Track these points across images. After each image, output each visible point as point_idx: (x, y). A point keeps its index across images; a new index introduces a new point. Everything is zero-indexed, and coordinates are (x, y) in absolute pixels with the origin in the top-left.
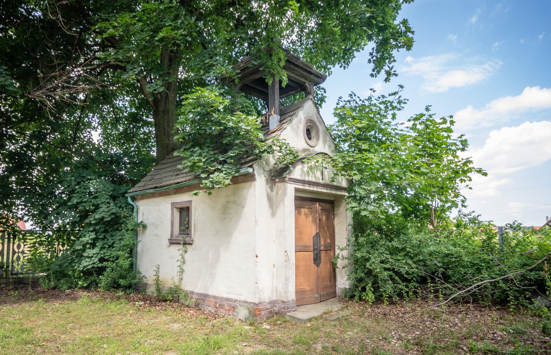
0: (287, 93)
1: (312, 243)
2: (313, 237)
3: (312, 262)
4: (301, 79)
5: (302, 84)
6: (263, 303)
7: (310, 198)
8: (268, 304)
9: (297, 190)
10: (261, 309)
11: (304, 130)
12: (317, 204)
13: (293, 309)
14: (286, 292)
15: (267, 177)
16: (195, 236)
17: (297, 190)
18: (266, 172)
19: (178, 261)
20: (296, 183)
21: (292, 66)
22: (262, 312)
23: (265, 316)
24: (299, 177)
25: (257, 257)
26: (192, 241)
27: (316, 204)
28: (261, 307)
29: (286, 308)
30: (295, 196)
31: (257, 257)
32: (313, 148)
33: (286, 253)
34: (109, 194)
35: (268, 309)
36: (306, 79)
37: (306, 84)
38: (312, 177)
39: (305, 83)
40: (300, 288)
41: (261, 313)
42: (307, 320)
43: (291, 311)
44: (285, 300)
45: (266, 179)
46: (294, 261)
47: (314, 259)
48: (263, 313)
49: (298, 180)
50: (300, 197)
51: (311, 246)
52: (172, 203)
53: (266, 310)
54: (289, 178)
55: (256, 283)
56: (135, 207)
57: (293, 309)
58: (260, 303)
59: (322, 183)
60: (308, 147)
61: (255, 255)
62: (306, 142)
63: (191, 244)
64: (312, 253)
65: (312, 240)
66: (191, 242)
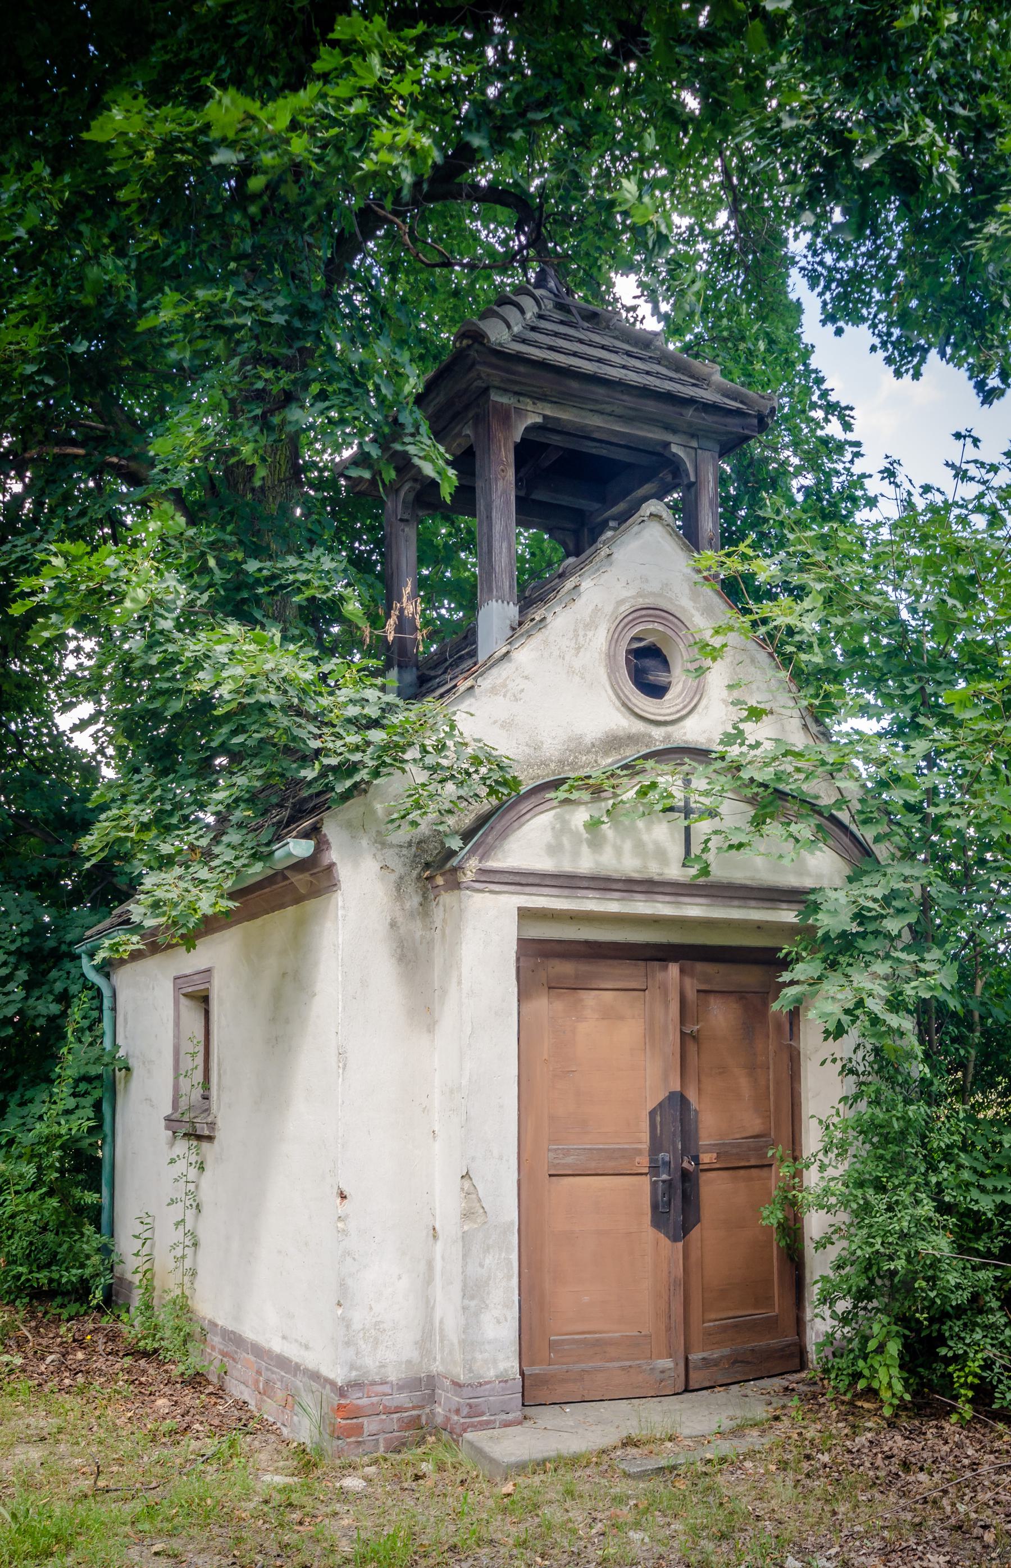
0: (628, 493)
1: (646, 1137)
2: (652, 1114)
3: (647, 1218)
4: (650, 435)
5: (659, 449)
6: (373, 1383)
7: (647, 946)
8: (401, 1388)
9: (525, 915)
10: (359, 1408)
11: (611, 658)
12: (673, 970)
13: (504, 1417)
14: (469, 1343)
15: (400, 870)
16: (219, 1109)
17: (525, 915)
18: (390, 852)
19: (172, 1202)
20: (528, 889)
21: (574, 385)
22: (365, 1421)
23: (381, 1438)
24: (545, 864)
25: (343, 1197)
26: (212, 1125)
27: (666, 968)
28: (365, 1401)
29: (465, 1411)
30: (521, 941)
31: (343, 1197)
32: (669, 729)
33: (467, 1184)
34: (13, 948)
35: (398, 1410)
36: (668, 428)
37: (674, 449)
38: (618, 851)
39: (667, 445)
40: (580, 1328)
41: (360, 1427)
42: (510, 1466)
43: (488, 1422)
44: (462, 1379)
45: (394, 877)
46: (512, 1215)
47: (655, 1207)
48: (370, 1425)
49: (544, 875)
50: (587, 943)
51: (638, 1152)
52: (176, 978)
53: (389, 1412)
54: (482, 871)
55: (339, 1304)
56: (106, 993)
57: (504, 1417)
58: (356, 1385)
59: (682, 879)
60: (639, 727)
61: (335, 1190)
62: (624, 704)
63: (210, 1138)
64: (645, 1182)
65: (645, 1125)
66: (206, 1133)
